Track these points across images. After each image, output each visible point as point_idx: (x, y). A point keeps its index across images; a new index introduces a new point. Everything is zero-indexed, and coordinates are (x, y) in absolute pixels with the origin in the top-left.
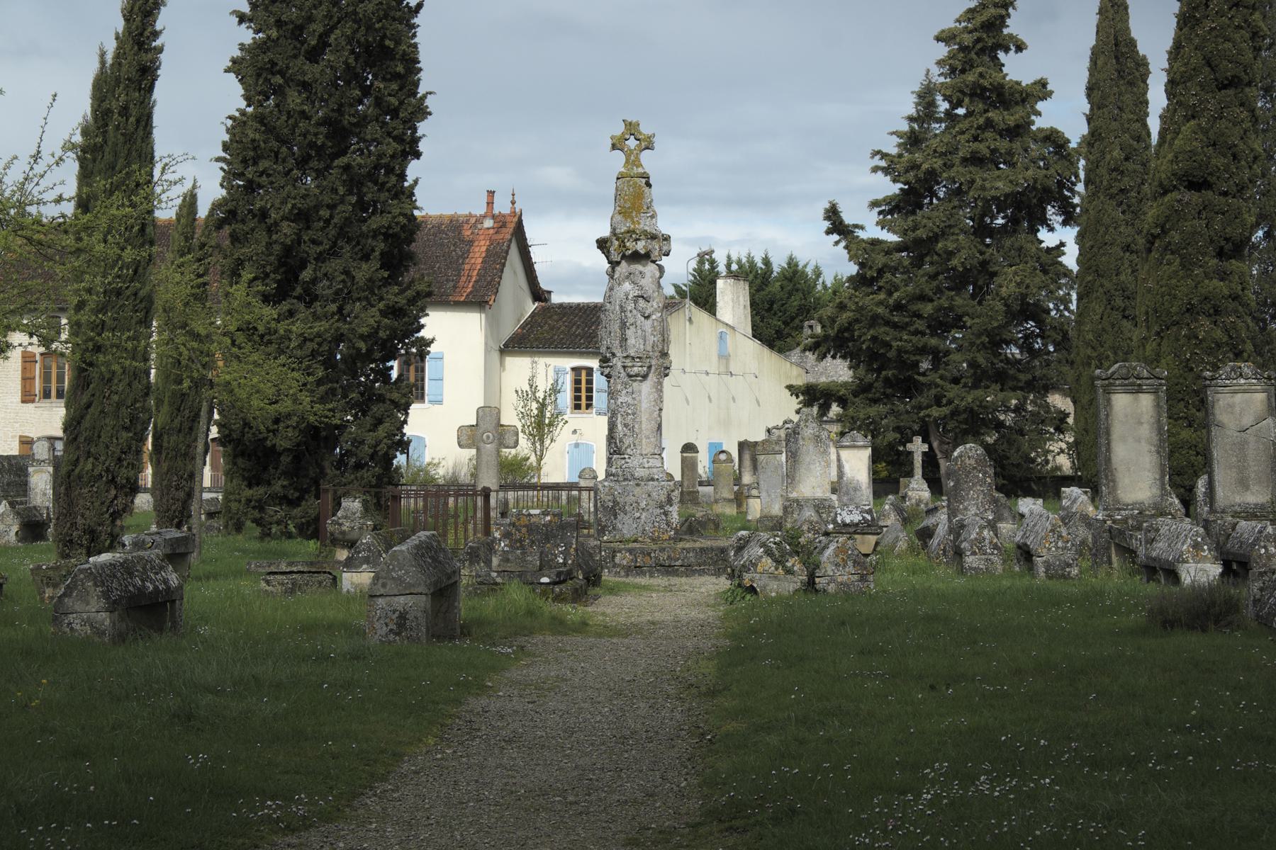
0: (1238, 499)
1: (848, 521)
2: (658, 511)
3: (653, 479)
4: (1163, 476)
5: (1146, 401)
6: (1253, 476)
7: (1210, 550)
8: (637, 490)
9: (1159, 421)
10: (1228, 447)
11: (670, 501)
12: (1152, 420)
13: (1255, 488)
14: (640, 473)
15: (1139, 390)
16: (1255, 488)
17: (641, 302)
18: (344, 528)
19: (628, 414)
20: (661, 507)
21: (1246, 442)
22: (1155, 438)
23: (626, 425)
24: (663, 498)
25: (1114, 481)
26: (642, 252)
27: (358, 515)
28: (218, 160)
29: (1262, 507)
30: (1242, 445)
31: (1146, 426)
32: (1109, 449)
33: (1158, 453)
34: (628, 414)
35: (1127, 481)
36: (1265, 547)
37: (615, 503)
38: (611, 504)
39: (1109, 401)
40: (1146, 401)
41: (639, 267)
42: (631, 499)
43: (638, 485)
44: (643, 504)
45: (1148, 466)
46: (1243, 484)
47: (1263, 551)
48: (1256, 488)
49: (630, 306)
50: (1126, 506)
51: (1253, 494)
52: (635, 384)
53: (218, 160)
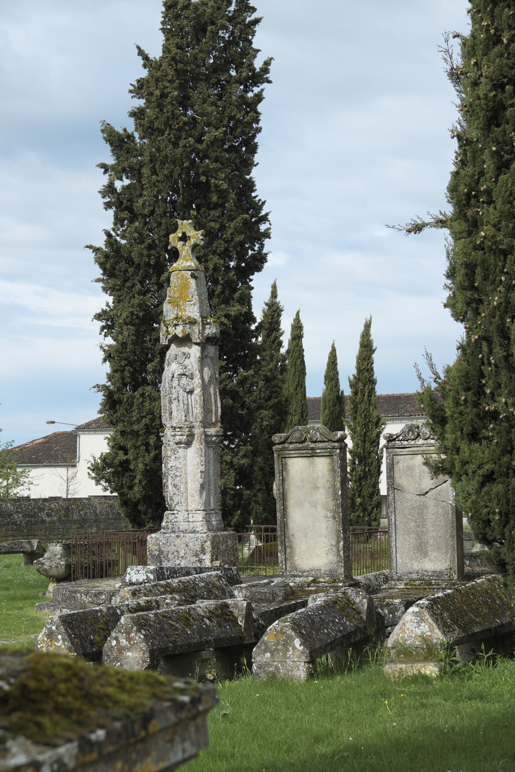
0: (416, 566)
1: (134, 580)
2: (194, 559)
3: (194, 532)
4: (338, 542)
5: (322, 465)
6: (431, 542)
7: (64, 640)
8: (178, 541)
9: (334, 486)
10: (407, 512)
11: (203, 551)
12: (328, 485)
13: (433, 554)
14: (183, 526)
15: (313, 454)
16: (433, 554)
17: (184, 380)
18: (45, 567)
19: (176, 476)
20: (197, 555)
21: (425, 506)
22: (331, 504)
23: (175, 486)
24: (198, 548)
25: (291, 547)
26: (180, 335)
27: (59, 556)
28: (98, 280)
29: (439, 575)
30: (421, 509)
31: (322, 491)
32: (285, 514)
33: (334, 518)
34: (176, 476)
35: (304, 547)
36: (116, 639)
37: (161, 551)
38: (157, 553)
39: (284, 466)
40: (322, 465)
41: (185, 349)
42: (172, 548)
43: (178, 537)
44: (182, 554)
45: (324, 532)
46: (421, 550)
47: (114, 643)
48: (435, 554)
49: (175, 383)
50: (302, 573)
51: (431, 560)
52: (181, 450)
53: (98, 280)
